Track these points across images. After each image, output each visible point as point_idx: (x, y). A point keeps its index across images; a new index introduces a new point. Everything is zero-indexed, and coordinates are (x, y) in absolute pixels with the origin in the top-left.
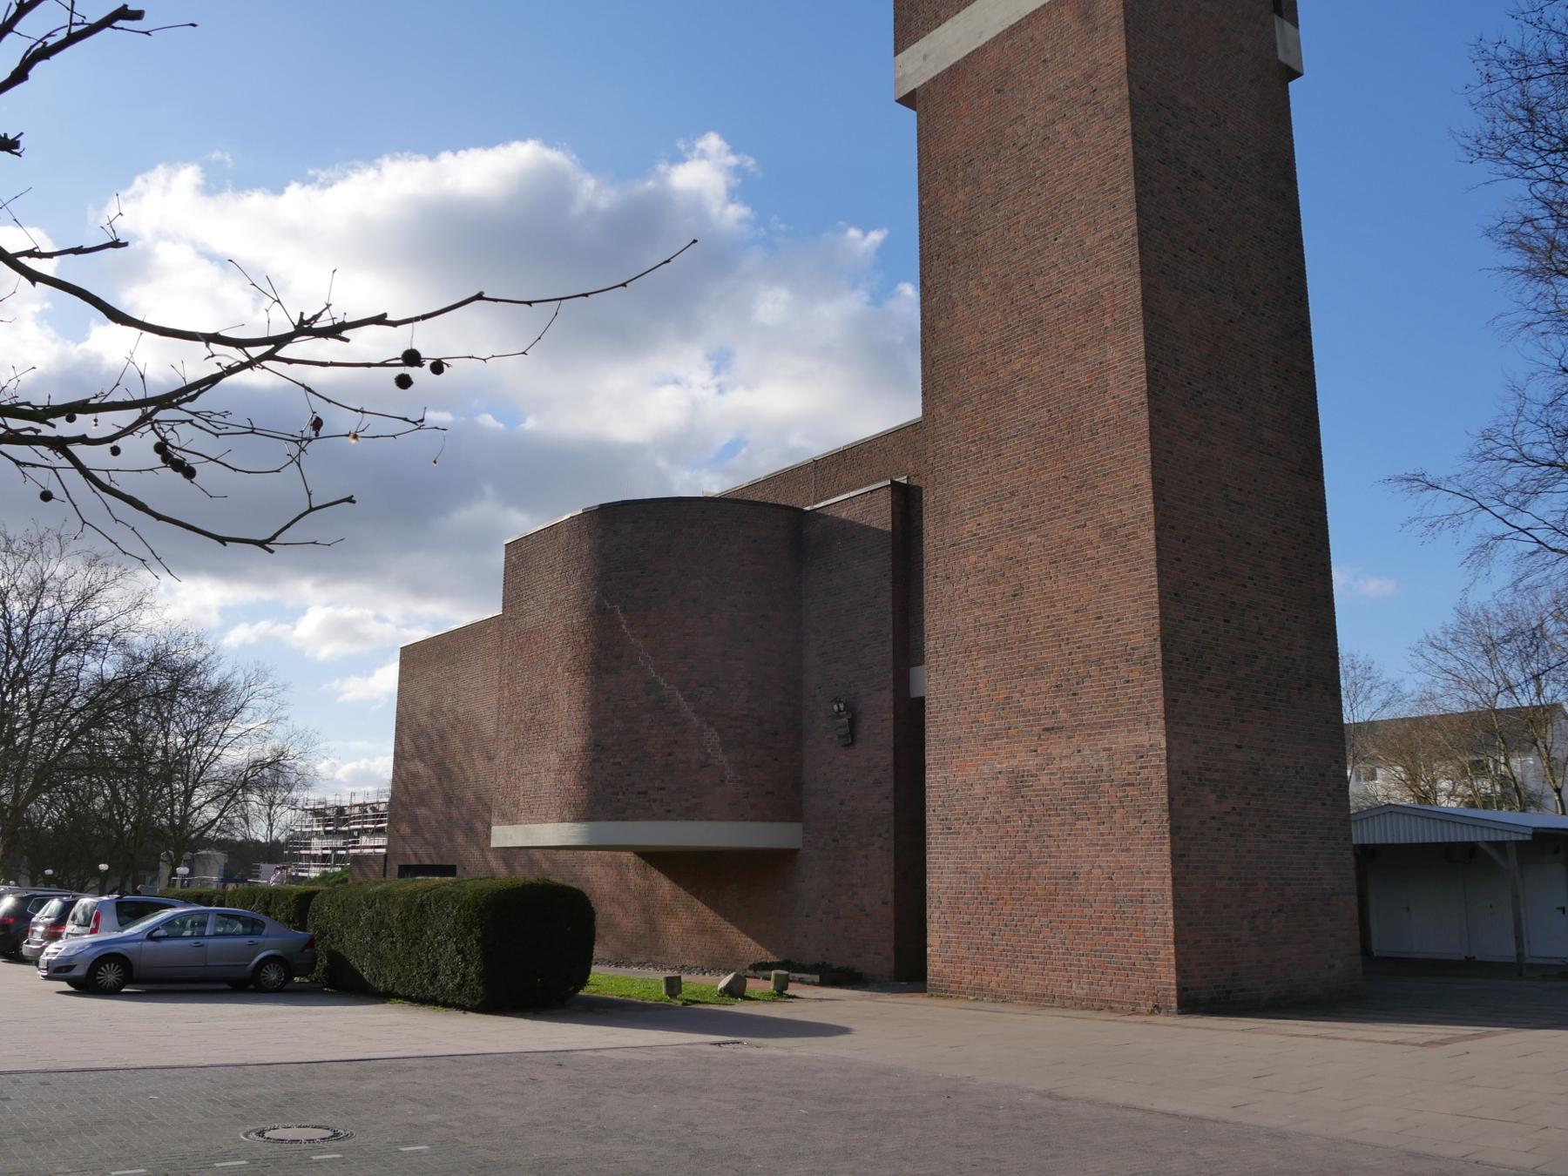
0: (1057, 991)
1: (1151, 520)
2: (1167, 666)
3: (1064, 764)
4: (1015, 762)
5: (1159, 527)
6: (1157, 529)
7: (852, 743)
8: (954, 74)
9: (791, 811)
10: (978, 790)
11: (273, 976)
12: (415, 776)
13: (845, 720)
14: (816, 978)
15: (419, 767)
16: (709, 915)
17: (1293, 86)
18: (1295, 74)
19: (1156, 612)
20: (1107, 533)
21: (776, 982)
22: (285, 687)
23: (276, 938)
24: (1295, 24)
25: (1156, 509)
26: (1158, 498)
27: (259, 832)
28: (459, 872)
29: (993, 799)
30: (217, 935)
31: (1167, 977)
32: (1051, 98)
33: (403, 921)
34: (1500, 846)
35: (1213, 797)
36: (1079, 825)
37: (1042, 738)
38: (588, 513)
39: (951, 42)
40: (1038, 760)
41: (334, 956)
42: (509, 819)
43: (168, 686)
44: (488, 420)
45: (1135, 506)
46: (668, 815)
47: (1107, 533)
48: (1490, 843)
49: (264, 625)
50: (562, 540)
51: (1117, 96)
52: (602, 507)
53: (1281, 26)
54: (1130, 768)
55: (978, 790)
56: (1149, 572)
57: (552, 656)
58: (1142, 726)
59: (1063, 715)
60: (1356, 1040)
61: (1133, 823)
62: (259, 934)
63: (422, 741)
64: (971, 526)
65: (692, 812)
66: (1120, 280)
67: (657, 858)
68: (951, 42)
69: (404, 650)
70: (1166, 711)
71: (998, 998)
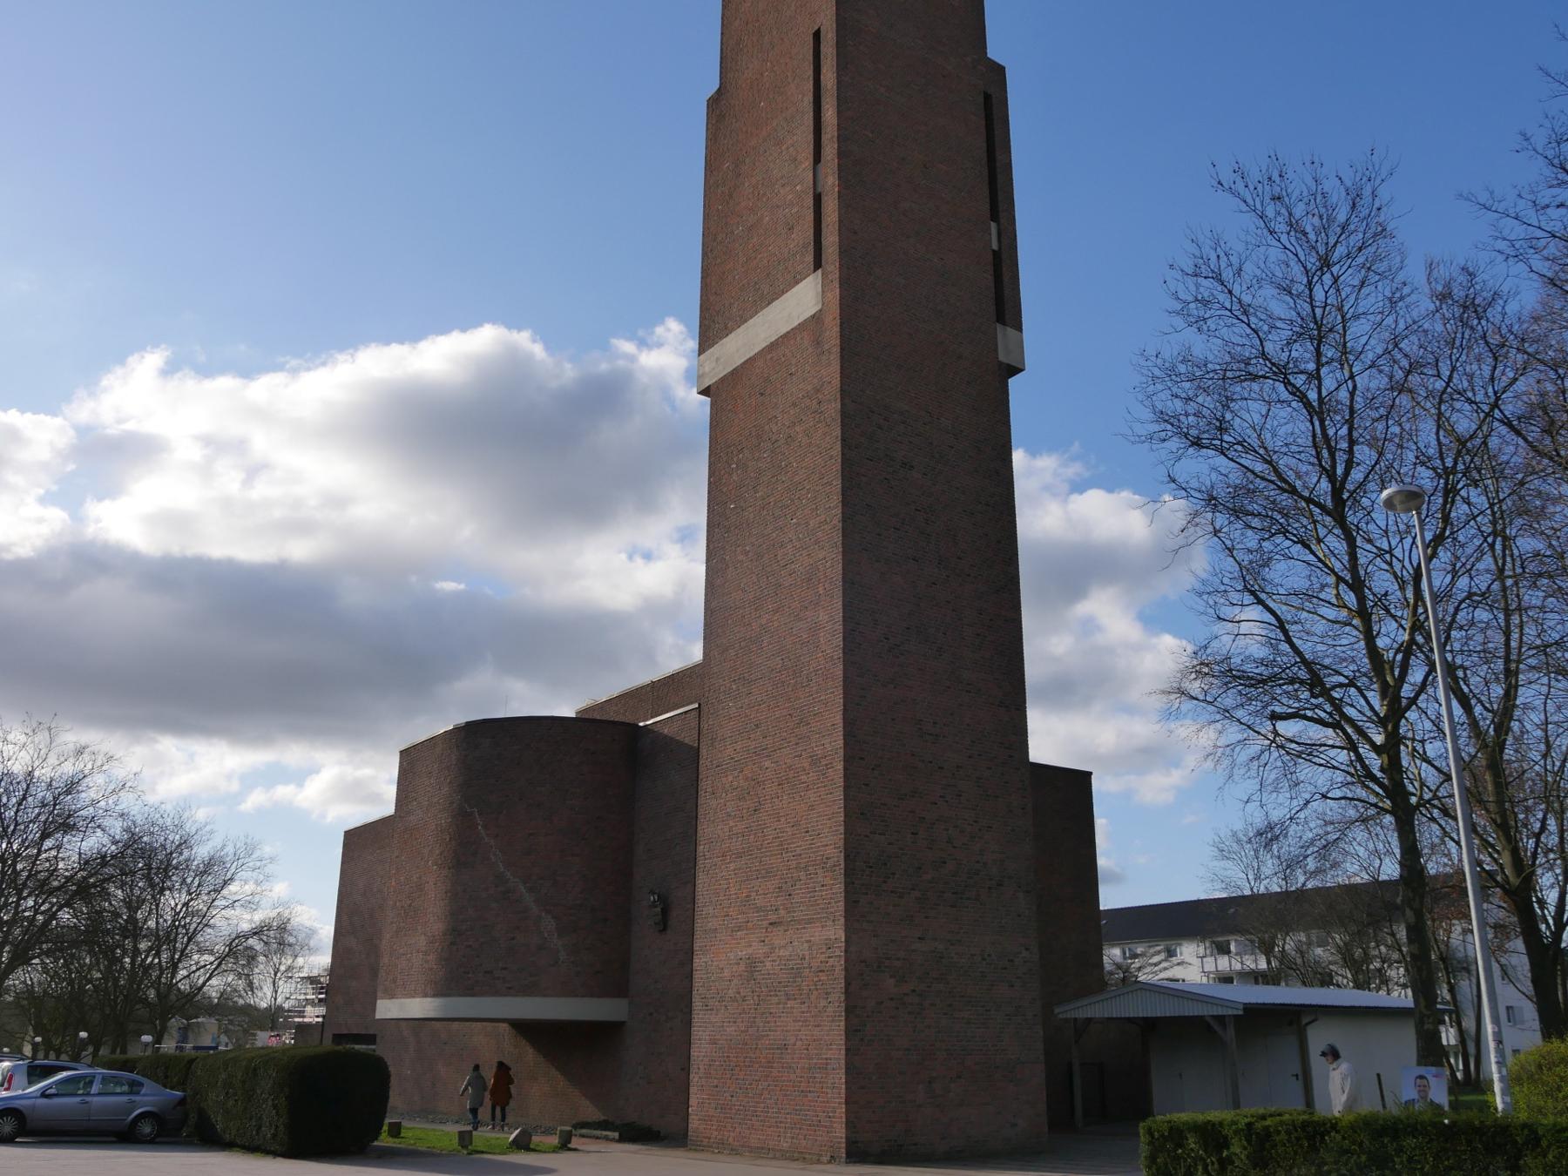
1: (841, 752)
2: (849, 873)
4: (750, 951)
5: (847, 760)
8: (735, 376)
9: (619, 989)
10: (726, 973)
11: (147, 1129)
14: (616, 1135)
17: (1013, 382)
18: (1015, 370)
19: (842, 829)
22: (272, 859)
23: (153, 1096)
24: (1019, 328)
25: (846, 744)
26: (848, 735)
29: (735, 981)
30: (99, 1094)
31: (840, 1132)
32: (794, 405)
33: (244, 1082)
34: (1220, 1019)
35: (892, 981)
37: (767, 927)
39: (742, 344)
40: (766, 949)
41: (202, 1113)
42: (391, 995)
43: (148, 861)
44: (449, 586)
45: (833, 743)
46: (510, 991)
49: (1064, 505)
51: (833, 408)
52: (468, 724)
53: (1004, 334)
55: (726, 973)
59: (782, 912)
61: (823, 1003)
62: (138, 1093)
65: (528, 990)
66: (829, 559)
67: (526, 1029)
68: (742, 344)
69: (348, 834)
70: (846, 911)
71: (734, 1152)
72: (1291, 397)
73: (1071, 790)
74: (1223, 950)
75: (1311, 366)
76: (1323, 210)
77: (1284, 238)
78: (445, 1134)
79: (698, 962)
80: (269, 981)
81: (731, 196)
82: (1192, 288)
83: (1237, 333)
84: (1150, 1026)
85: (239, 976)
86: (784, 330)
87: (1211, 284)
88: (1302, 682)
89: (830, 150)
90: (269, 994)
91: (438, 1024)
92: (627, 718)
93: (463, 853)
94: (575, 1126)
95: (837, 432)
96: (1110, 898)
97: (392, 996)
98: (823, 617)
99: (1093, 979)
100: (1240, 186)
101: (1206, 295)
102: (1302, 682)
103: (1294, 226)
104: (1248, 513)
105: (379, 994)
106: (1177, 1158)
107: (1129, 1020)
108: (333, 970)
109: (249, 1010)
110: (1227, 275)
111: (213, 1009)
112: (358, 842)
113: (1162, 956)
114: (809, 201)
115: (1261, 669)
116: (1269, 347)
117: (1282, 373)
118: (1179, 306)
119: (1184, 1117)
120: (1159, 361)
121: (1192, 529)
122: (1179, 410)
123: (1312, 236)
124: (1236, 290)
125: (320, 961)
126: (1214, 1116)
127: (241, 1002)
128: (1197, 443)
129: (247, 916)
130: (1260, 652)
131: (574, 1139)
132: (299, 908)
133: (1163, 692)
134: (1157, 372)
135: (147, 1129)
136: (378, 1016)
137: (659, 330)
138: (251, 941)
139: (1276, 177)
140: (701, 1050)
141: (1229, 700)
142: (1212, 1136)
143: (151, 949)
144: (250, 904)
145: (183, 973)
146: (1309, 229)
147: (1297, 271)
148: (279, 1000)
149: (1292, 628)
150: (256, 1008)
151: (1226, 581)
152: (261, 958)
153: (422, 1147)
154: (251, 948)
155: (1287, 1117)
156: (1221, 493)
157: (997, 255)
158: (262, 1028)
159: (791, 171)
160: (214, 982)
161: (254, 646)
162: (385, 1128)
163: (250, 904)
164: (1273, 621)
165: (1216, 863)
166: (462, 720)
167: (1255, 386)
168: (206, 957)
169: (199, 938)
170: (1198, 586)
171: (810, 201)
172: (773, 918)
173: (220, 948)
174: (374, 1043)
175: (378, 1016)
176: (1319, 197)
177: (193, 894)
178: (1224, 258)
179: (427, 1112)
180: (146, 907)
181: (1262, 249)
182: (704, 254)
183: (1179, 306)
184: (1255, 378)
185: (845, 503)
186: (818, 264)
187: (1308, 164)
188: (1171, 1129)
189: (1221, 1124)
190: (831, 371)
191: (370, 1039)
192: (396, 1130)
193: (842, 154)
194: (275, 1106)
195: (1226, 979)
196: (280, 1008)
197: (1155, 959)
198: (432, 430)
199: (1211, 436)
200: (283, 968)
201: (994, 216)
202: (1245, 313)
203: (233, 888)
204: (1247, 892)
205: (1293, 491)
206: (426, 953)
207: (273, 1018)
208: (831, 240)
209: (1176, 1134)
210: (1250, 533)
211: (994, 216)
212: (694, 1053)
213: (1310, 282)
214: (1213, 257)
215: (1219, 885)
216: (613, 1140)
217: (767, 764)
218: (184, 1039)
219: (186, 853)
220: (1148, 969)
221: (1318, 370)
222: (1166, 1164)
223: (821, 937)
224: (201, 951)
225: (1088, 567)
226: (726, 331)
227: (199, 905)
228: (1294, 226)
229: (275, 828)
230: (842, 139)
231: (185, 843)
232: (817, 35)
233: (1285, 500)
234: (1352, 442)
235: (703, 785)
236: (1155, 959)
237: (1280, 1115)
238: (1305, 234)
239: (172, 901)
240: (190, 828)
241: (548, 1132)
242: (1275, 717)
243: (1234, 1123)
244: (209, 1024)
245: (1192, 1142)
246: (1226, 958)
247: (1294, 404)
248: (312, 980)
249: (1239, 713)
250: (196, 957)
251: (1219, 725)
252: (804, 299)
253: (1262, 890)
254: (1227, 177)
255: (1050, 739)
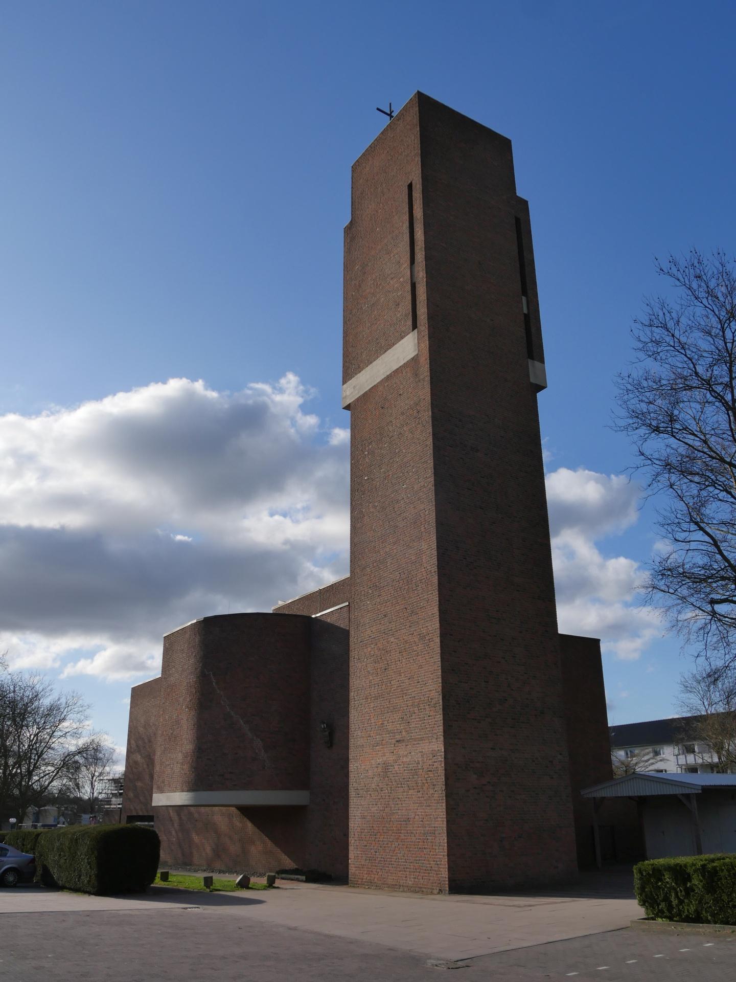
0: (402, 882)
1: (438, 632)
3: (405, 760)
5: (442, 636)
6: (441, 636)
7: (331, 746)
8: (365, 397)
10: (370, 773)
12: (136, 762)
13: (327, 733)
14: (304, 878)
15: (138, 758)
16: (269, 843)
17: (539, 395)
18: (541, 388)
19: (440, 680)
20: (422, 637)
21: (268, 879)
22: (89, 706)
24: (543, 362)
27: (86, 793)
28: (155, 819)
29: (376, 779)
31: (445, 874)
32: (403, 414)
33: (70, 848)
34: (687, 796)
36: (411, 792)
37: (396, 744)
38: (198, 623)
39: (370, 376)
40: (394, 757)
41: (46, 869)
42: (161, 791)
44: (179, 538)
45: (433, 625)
46: (235, 787)
47: (422, 637)
48: (682, 795)
50: (187, 636)
51: (427, 415)
53: (533, 365)
54: (430, 762)
56: (437, 658)
57: (181, 699)
58: (434, 740)
60: (485, 904)
61: (431, 791)
63: (140, 742)
64: (369, 632)
65: (247, 785)
67: (247, 811)
68: (370, 376)
70: (444, 732)
71: (378, 887)
72: (714, 400)
73: (588, 649)
74: (690, 750)
75: (727, 379)
76: (727, 283)
77: (705, 301)
78: (193, 880)
79: (352, 766)
80: (89, 782)
81: (360, 286)
82: (649, 334)
83: (678, 361)
84: (642, 801)
85: (70, 780)
86: (395, 368)
87: (661, 332)
88: (729, 579)
89: (420, 256)
90: (89, 790)
91: (192, 809)
92: (305, 613)
93: (205, 700)
94: (278, 873)
95: (430, 430)
96: (616, 718)
97: (162, 791)
98: (424, 546)
99: (604, 770)
100: (674, 270)
101: (658, 338)
102: (729, 579)
103: (710, 293)
104: (691, 474)
105: (154, 790)
106: (659, 888)
107: (630, 798)
108: (126, 774)
109: (78, 800)
110: (670, 324)
111: (53, 800)
112: (140, 694)
113: (651, 755)
114: (408, 287)
115: (702, 572)
116: (700, 369)
117: (708, 384)
118: (641, 346)
119: (662, 861)
120: (630, 380)
121: (655, 485)
122: (645, 410)
123: (722, 299)
124: (677, 334)
125: (119, 769)
126: (682, 860)
127: (72, 796)
128: (657, 430)
129: (74, 742)
130: (700, 560)
131: (277, 881)
132: (106, 737)
133: (644, 587)
134: (630, 387)
135: (11, 878)
136: (154, 804)
137: (283, 381)
138: (77, 758)
139: (696, 264)
140: (356, 822)
141: (684, 591)
142: (681, 874)
143: (15, 763)
144: (76, 734)
145: (36, 778)
146: (720, 295)
147: (714, 321)
148: (95, 794)
149: (723, 546)
150: (80, 799)
151: (679, 516)
152: (83, 769)
153: (181, 887)
154: (76, 762)
155: (727, 860)
156: (674, 460)
157: (527, 317)
158: (85, 813)
159: (398, 267)
160: (55, 783)
161: (63, 579)
162: (158, 875)
163: (76, 734)
164: (711, 541)
165: (683, 695)
166: (201, 618)
167: (689, 393)
168: (49, 768)
169: (45, 756)
170: (661, 519)
171: (409, 288)
172: (398, 737)
173: (58, 762)
174: (152, 821)
175: (154, 804)
176: (725, 274)
177: (41, 729)
178: (667, 315)
179: (186, 864)
180: (11, 738)
181: (692, 308)
182: (345, 323)
183: (641, 346)
184: (691, 388)
185: (435, 474)
186: (415, 326)
187: (716, 255)
188: (654, 869)
189: (686, 866)
190: (425, 393)
191: (150, 818)
192: (165, 877)
193: (427, 258)
194: (89, 863)
195: (693, 770)
196: (97, 798)
197: (646, 758)
198: (144, 445)
199: (668, 425)
200: (97, 774)
201: (524, 292)
202: (683, 348)
203: (65, 724)
204: (704, 713)
205: (722, 460)
206: (182, 764)
207: (92, 806)
208: (422, 311)
209: (657, 873)
210: (693, 485)
211: (524, 292)
212: (351, 824)
213: (723, 328)
214: (661, 314)
215: (686, 709)
216: (302, 881)
217: (392, 639)
218: (37, 820)
219: (36, 703)
220: (642, 764)
221: (731, 381)
222: (651, 892)
223: (428, 748)
224: (47, 764)
225: (577, 516)
226: (359, 369)
227: (44, 735)
228: (710, 293)
229: (95, 686)
230: (427, 248)
231: (36, 696)
232: (410, 186)
233: (714, 463)
234: (705, 442)
235: (352, 654)
236: (646, 758)
237: (724, 859)
238: (717, 298)
239: (29, 733)
240: (39, 688)
241: (261, 875)
242: (713, 602)
243: (693, 865)
244: (52, 810)
245: (667, 877)
246: (692, 755)
247: (717, 404)
248: (115, 781)
249: (692, 600)
250: (43, 768)
251: (679, 607)
252: (408, 348)
253: (713, 711)
254: (666, 266)
255: (572, 618)
